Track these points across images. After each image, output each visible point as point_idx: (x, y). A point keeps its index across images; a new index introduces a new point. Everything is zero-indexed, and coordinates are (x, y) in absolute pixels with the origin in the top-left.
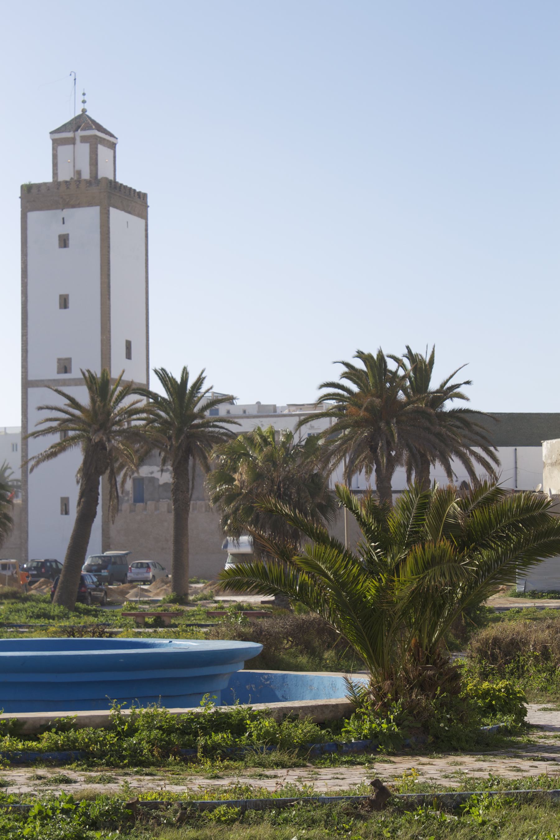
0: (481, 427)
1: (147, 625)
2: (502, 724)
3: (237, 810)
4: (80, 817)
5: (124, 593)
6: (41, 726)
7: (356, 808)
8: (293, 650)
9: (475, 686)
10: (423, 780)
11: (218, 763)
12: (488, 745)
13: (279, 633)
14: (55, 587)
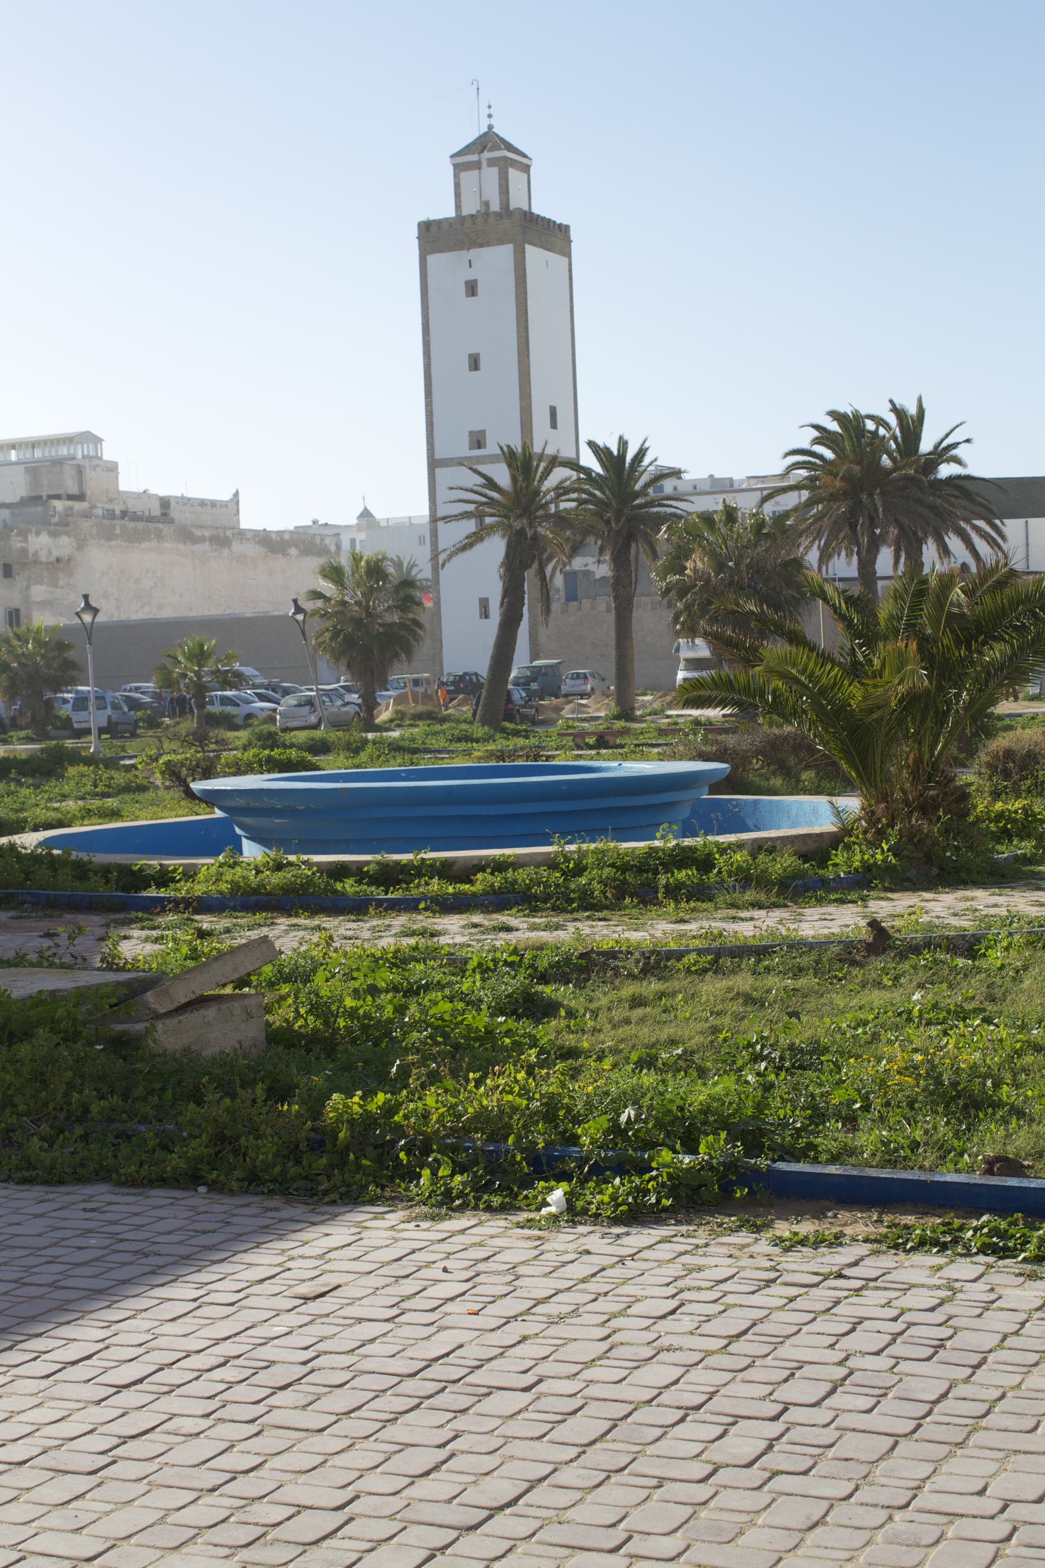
0: (983, 498)
1: (590, 747)
2: (1019, 852)
3: (709, 958)
4: (527, 969)
5: (558, 709)
6: (474, 866)
7: (850, 953)
8: (764, 771)
9: (986, 807)
10: (928, 919)
11: (683, 905)
12: (1003, 876)
13: (747, 751)
14: (477, 705)
